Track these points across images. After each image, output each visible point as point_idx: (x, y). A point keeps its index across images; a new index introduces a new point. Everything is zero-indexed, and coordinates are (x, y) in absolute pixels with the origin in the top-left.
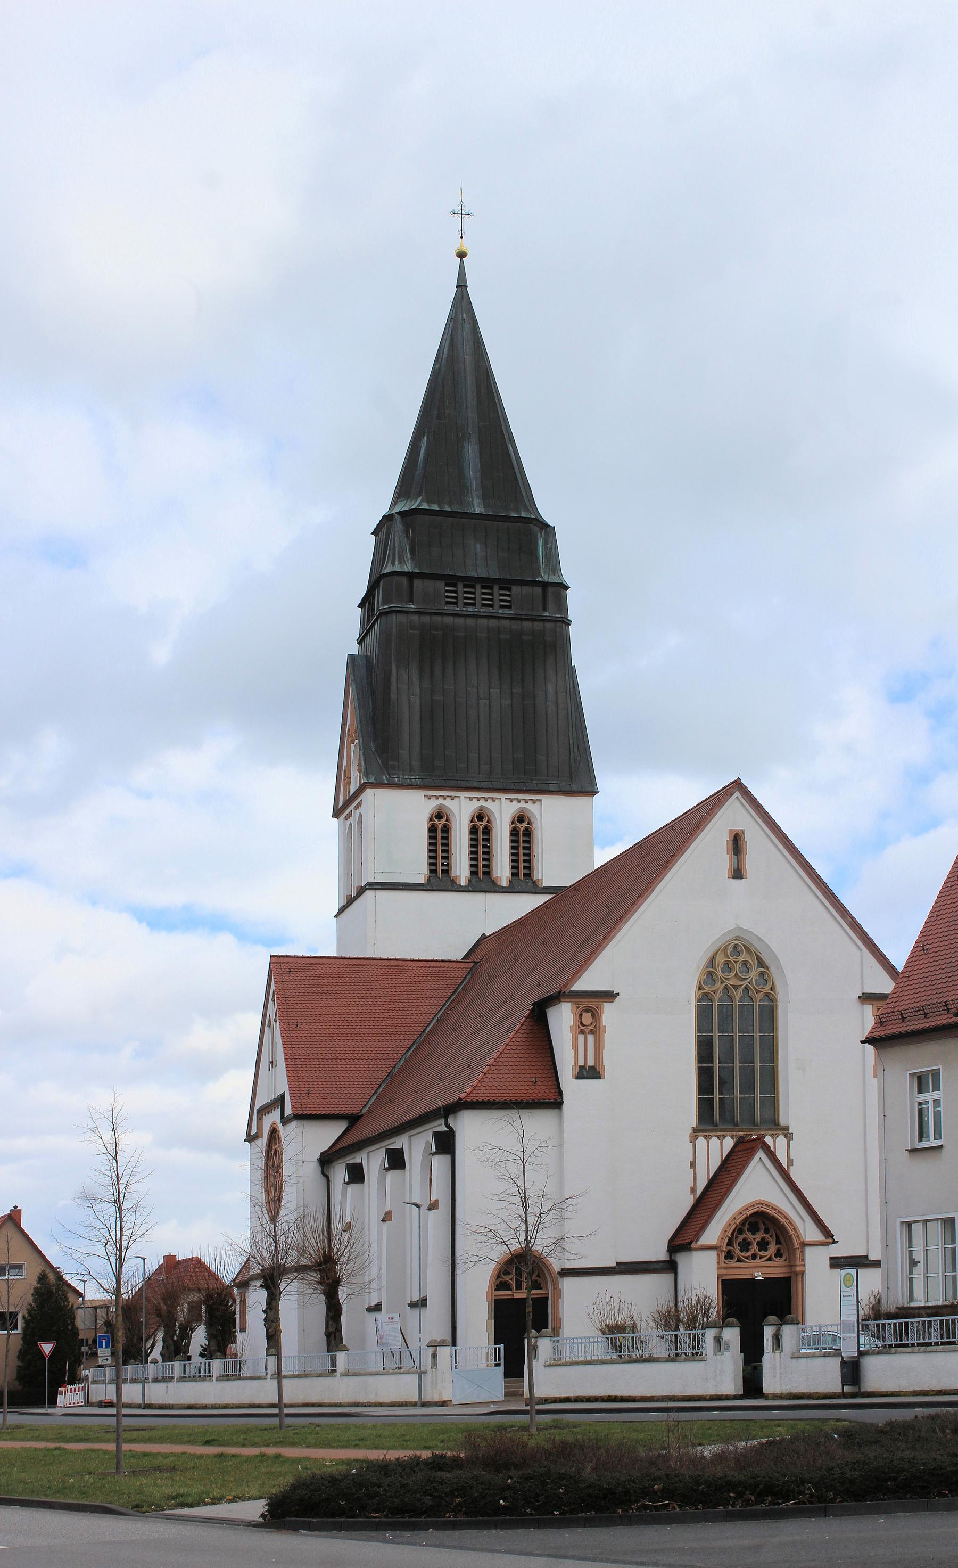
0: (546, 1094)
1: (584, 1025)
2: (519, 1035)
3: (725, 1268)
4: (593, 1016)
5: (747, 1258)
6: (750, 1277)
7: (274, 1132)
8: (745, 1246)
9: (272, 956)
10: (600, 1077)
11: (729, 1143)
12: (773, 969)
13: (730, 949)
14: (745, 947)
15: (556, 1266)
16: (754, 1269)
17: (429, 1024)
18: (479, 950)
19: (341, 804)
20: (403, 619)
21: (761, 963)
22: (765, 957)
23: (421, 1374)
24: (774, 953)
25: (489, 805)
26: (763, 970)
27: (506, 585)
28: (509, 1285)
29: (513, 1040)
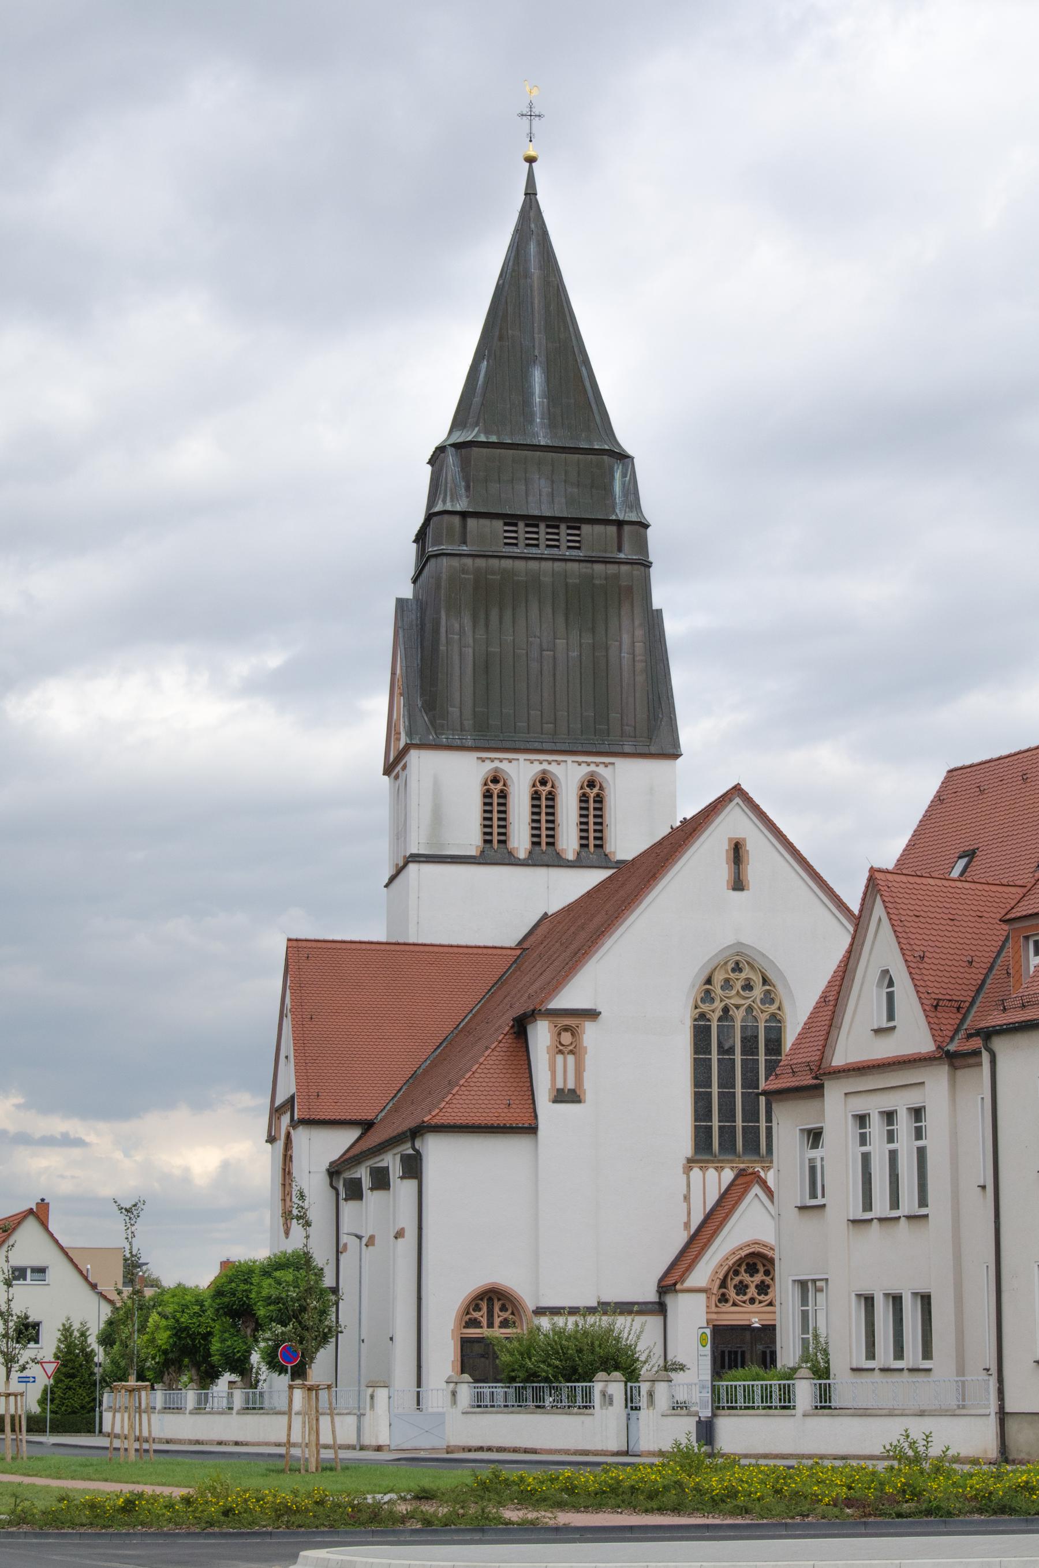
0: (517, 1116)
1: (563, 1045)
2: (496, 1053)
3: (716, 1313)
4: (573, 1035)
5: (744, 1302)
6: (747, 1323)
7: (288, 1136)
8: (742, 1288)
9: (289, 940)
10: (579, 1101)
11: (728, 1175)
12: (780, 989)
13: (731, 965)
14: (748, 963)
15: (530, 1305)
16: (751, 1315)
17: (463, 1020)
18: (536, 932)
19: (391, 759)
20: (455, 562)
21: (765, 981)
22: (771, 975)
23: (360, 1416)
24: (779, 970)
25: (553, 768)
26: (768, 987)
27: (575, 523)
28: (480, 1322)
29: (489, 1058)
